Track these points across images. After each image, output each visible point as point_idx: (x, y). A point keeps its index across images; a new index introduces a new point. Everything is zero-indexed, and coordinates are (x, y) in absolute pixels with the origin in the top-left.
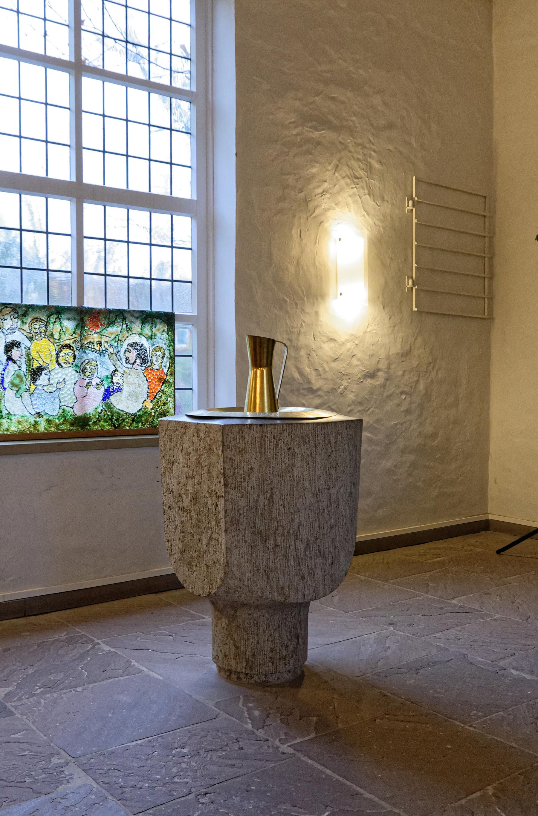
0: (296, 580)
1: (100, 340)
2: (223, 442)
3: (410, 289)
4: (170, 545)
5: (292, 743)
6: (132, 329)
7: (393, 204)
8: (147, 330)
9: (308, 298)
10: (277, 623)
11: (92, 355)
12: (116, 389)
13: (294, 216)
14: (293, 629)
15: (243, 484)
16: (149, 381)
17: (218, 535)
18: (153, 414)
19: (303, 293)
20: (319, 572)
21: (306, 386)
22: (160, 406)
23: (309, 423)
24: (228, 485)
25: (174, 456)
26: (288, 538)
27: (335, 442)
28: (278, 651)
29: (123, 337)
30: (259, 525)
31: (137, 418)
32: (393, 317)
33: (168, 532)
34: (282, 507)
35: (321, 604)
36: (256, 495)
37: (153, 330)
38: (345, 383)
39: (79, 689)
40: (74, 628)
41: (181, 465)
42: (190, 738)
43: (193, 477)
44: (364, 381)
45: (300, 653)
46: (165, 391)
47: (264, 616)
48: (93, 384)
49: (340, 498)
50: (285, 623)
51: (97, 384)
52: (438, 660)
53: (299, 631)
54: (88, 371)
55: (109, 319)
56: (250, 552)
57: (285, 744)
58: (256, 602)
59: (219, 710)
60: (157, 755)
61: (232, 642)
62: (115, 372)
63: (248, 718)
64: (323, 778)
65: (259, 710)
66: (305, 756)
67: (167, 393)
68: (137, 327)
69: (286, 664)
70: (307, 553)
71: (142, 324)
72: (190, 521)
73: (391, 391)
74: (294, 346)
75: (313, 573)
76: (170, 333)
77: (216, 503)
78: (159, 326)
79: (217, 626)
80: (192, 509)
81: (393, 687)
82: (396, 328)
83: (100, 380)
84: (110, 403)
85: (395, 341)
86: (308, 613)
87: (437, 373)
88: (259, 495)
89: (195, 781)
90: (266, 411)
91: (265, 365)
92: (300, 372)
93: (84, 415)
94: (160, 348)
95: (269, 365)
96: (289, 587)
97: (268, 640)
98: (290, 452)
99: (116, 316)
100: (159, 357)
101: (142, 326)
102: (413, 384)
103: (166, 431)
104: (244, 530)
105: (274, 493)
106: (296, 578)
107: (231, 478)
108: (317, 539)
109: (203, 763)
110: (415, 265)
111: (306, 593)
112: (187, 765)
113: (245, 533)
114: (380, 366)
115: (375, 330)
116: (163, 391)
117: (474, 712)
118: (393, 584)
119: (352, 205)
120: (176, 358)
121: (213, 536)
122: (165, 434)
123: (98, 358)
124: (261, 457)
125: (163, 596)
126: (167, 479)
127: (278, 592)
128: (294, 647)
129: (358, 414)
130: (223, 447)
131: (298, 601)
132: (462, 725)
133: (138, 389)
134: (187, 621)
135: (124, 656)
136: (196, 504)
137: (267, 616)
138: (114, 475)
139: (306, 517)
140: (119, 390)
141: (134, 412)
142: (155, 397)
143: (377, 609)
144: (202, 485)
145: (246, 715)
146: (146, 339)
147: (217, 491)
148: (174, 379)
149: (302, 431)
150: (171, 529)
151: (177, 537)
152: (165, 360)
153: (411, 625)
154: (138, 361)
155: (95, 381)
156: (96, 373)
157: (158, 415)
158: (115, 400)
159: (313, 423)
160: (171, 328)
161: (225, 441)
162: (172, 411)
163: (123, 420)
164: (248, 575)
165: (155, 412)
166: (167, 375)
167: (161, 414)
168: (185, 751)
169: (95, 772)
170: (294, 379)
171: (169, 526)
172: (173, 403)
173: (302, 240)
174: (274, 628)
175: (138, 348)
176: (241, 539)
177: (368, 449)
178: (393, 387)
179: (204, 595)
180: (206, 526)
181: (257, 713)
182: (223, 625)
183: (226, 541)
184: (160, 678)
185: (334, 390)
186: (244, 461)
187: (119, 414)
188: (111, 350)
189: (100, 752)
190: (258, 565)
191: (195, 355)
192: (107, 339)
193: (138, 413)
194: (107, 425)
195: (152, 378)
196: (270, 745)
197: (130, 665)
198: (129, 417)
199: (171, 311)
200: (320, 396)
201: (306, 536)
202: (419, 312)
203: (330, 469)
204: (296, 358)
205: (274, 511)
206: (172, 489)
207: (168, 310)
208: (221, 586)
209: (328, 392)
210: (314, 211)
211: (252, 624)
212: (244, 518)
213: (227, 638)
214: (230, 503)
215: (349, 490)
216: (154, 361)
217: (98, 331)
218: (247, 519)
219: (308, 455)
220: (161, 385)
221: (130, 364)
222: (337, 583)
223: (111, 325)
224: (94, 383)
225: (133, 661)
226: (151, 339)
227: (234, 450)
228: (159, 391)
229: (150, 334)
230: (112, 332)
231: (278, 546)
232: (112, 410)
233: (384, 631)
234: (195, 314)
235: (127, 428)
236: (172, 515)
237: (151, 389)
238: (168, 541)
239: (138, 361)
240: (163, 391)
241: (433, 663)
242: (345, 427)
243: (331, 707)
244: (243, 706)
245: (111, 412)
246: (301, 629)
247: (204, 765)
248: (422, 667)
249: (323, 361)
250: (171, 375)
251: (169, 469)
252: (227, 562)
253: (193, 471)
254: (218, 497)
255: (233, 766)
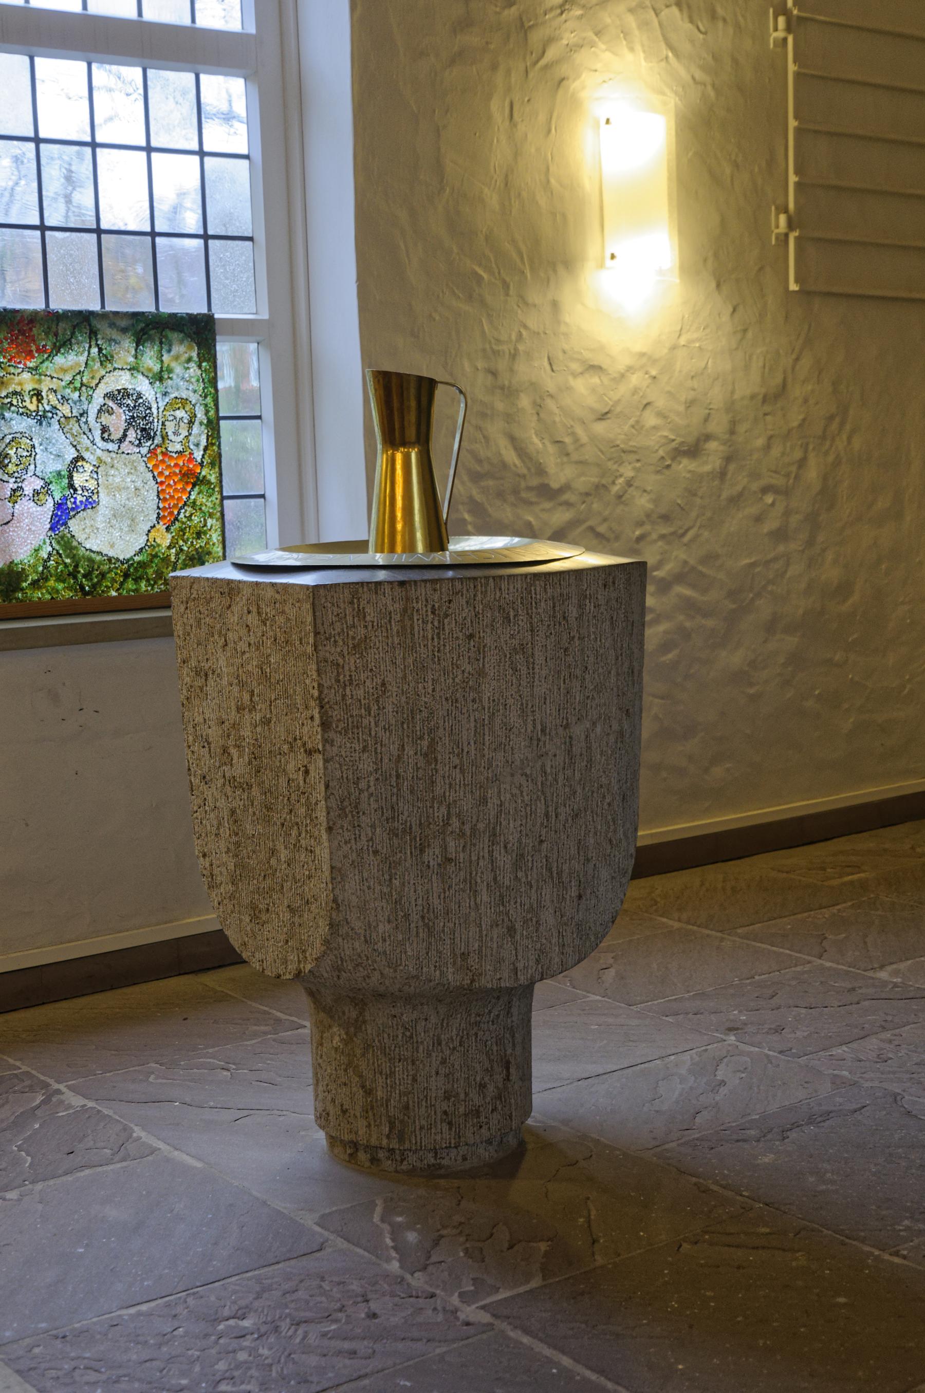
0: (495, 936)
1: (36, 386)
3: (782, 238)
4: (207, 865)
6: (112, 357)
8: (150, 360)
10: (457, 1035)
11: (20, 424)
12: (81, 502)
13: (494, 67)
14: (495, 1048)
16: (159, 480)
18: (173, 558)
20: (548, 918)
21: (535, 482)
22: (188, 539)
24: (331, 723)
25: (207, 660)
26: (474, 841)
27: (579, 618)
28: (462, 1096)
29: (93, 378)
30: (406, 813)
31: (136, 569)
33: (203, 835)
34: (458, 770)
35: (574, 988)
36: (396, 746)
37: (164, 358)
38: (628, 472)
39: (12, 1195)
40: (5, 1057)
41: (225, 682)
42: (258, 1296)
43: (253, 709)
44: (674, 466)
45: (513, 1101)
46: (198, 503)
47: (426, 1020)
48: (26, 493)
49: (594, 746)
50: (476, 1034)
51: (36, 493)
53: (509, 1051)
54: (13, 461)
55: (56, 335)
56: (387, 877)
57: (474, 1303)
59: (326, 1233)
60: (182, 1333)
62: (77, 462)
63: (392, 1247)
64: (553, 1374)
65: (415, 1230)
66: (516, 1327)
67: (203, 508)
68: (125, 351)
69: (481, 1127)
70: (520, 874)
71: (137, 346)
73: (739, 488)
74: (502, 388)
75: (534, 919)
76: (204, 364)
77: (306, 766)
78: (178, 349)
79: (322, 1045)
80: (253, 780)
82: (750, 335)
83: (42, 483)
84: (69, 535)
85: (747, 368)
88: (403, 745)
90: (420, 547)
93: (9, 566)
95: (423, 440)
96: (480, 951)
97: (437, 1073)
98: (472, 643)
99: (74, 327)
100: (182, 424)
101: (136, 350)
102: (794, 469)
104: (371, 826)
106: (495, 932)
108: (541, 841)
109: (285, 1349)
111: (520, 965)
112: (250, 1356)
113: (373, 834)
114: (712, 427)
115: (698, 340)
116: (194, 502)
117: (906, 1222)
119: (636, 32)
120: (222, 423)
121: (303, 842)
122: (187, 608)
124: (404, 658)
127: (454, 963)
128: (497, 1087)
129: (660, 543)
132: (877, 1253)
133: (134, 503)
134: (265, 1033)
135: (117, 1118)
137: (433, 1019)
138: (84, 707)
139: (515, 791)
140: (90, 504)
141: (128, 556)
142: (176, 519)
143: (703, 995)
145: (389, 1242)
146: (147, 382)
147: (305, 738)
148: (221, 474)
149: (498, 594)
150: (209, 828)
151: (223, 845)
152: (196, 429)
153: (779, 1030)
154: (132, 435)
155: (31, 485)
156: (32, 467)
157: (184, 560)
158: (81, 528)
159: (526, 575)
160: (208, 354)
161: (319, 621)
162: (218, 549)
163: (103, 575)
165: (177, 554)
166: (201, 464)
167: (192, 559)
168: (246, 1323)
169: (44, 1375)
170: (504, 465)
171: (204, 822)
173: (515, 126)
174: (451, 1046)
175: (129, 402)
177: (688, 624)
179: (288, 977)
180: (285, 820)
181: (412, 1237)
182: (334, 1042)
183: (331, 853)
184: (199, 1165)
185: (600, 489)
186: (365, 667)
187: (91, 560)
188: (65, 410)
189: (54, 1332)
190: (407, 905)
191: (268, 414)
192: (54, 384)
193: (137, 558)
194: (64, 588)
195: (167, 473)
197: (131, 1136)
198: (116, 568)
199: (204, 310)
200: (568, 504)
201: (517, 835)
205: (439, 780)
206: (207, 735)
207: (199, 308)
208: (324, 954)
209: (588, 494)
210: (544, 53)
211: (400, 1037)
213: (345, 1070)
214: (338, 766)
216: (170, 433)
217: (31, 364)
218: (377, 801)
219: (515, 649)
220: (189, 489)
221: (112, 441)
222: (593, 939)
223: (62, 351)
224: (28, 490)
225: (136, 1128)
226: (161, 379)
227: (341, 643)
228: (185, 504)
229: (157, 368)
230: (65, 367)
231: (450, 860)
234: (265, 315)
235: (114, 594)
236: (210, 797)
237: (165, 500)
238: (204, 856)
239: (132, 435)
240: (194, 502)
242: (600, 583)
243: (582, 1220)
244: (383, 1220)
245: (73, 557)
246: (514, 1045)
248: (795, 1125)
249: (573, 420)
250: (212, 464)
251: (198, 690)
252: (335, 900)
253: (252, 694)
254: (309, 753)
255: (353, 1353)
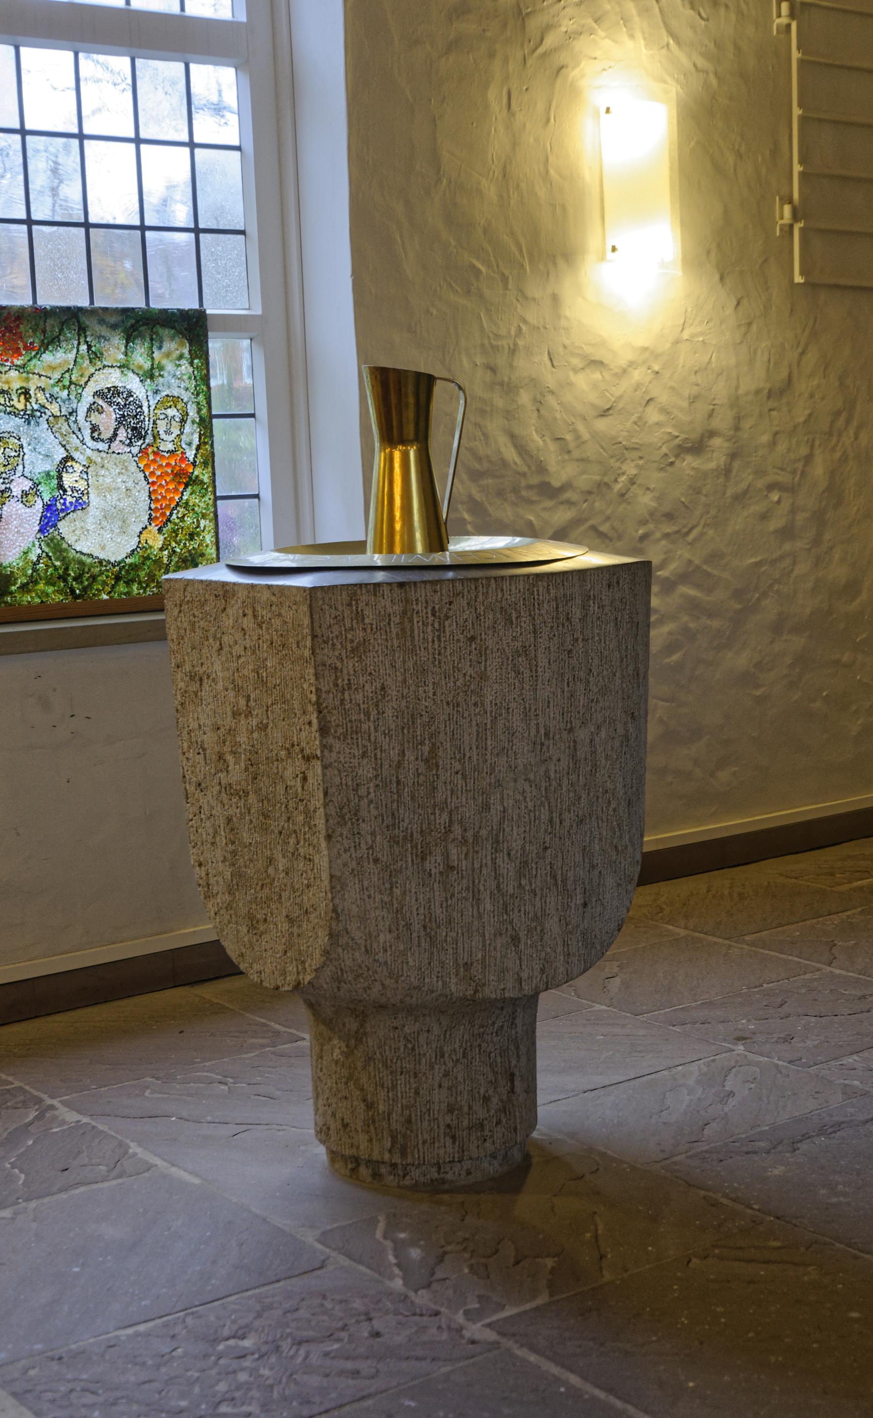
0: (499, 946)
1: (24, 385)
2: (313, 630)
3: (787, 229)
4: (203, 874)
5: (494, 1318)
6: (102, 354)
7: (740, 12)
8: (140, 357)
9: (531, 262)
10: (460, 1047)
12: (71, 503)
13: (492, 55)
15: (365, 727)
16: (150, 480)
17: (311, 849)
18: (165, 560)
19: (521, 251)
20: (553, 925)
21: (535, 480)
22: (180, 541)
23: (516, 576)
25: (202, 664)
27: (583, 619)
28: (466, 1109)
29: (82, 376)
30: (407, 821)
31: (127, 572)
32: (745, 301)
33: (199, 844)
34: (460, 776)
35: (579, 997)
36: (397, 751)
38: (630, 469)
41: (220, 686)
42: (259, 1315)
43: (249, 714)
44: (677, 463)
45: (518, 1114)
46: (191, 504)
48: (15, 494)
49: (599, 750)
50: (480, 1046)
51: (25, 494)
52: (844, 1119)
53: (514, 1062)
55: (44, 332)
56: (387, 886)
58: (408, 999)
59: (327, 1250)
61: (358, 1093)
62: (66, 462)
64: (562, 1394)
67: (196, 509)
69: (485, 1140)
70: (523, 882)
71: (127, 343)
72: (247, 818)
73: (743, 486)
74: (502, 384)
75: (539, 928)
76: (196, 361)
77: (304, 773)
78: (170, 345)
79: (321, 1057)
80: (250, 787)
81: (736, 1185)
82: (754, 327)
83: (30, 484)
85: (751, 362)
86: (535, 1021)
87: (856, 436)
89: (267, 1411)
90: (419, 548)
91: (411, 436)
92: (521, 449)
94: (175, 400)
97: (440, 1086)
98: (474, 646)
99: (63, 324)
100: (173, 423)
101: (126, 347)
102: (800, 465)
103: (181, 606)
105: (438, 744)
107: (335, 712)
110: (797, 168)
111: (524, 975)
112: (251, 1376)
113: (373, 841)
114: (716, 423)
115: (701, 334)
116: (187, 503)
118: (752, 944)
119: (637, 19)
120: (214, 421)
121: (301, 851)
122: (180, 612)
123: (24, 428)
124: (404, 661)
125: (207, 992)
126: (191, 720)
128: (501, 1100)
129: (664, 542)
130: (313, 639)
131: (507, 995)
133: (125, 503)
136: (259, 777)
139: (519, 797)
140: (81, 505)
141: (119, 558)
142: (169, 520)
143: (710, 1004)
144: (269, 730)
145: (392, 1259)
146: (138, 379)
148: (214, 474)
149: (500, 595)
150: (204, 836)
151: (219, 854)
152: (188, 428)
154: (122, 434)
156: (20, 468)
157: (177, 562)
159: (528, 576)
161: (316, 625)
162: (211, 551)
163: (94, 578)
164: (385, 938)
165: (170, 556)
166: (194, 464)
167: (184, 561)
168: (247, 1343)
170: (504, 463)
171: (200, 831)
172: (212, 533)
173: (513, 115)
175: (120, 400)
176: (366, 856)
177: (692, 625)
178: (749, 474)
179: (287, 988)
180: (283, 827)
182: (335, 1054)
183: (330, 861)
184: (197, 1181)
185: (602, 487)
187: (81, 563)
188: (54, 408)
189: (50, 1354)
191: (262, 411)
192: (43, 382)
193: (128, 561)
194: (54, 592)
195: (158, 473)
196: (444, 1322)
197: (126, 1153)
198: (107, 571)
199: (196, 306)
200: (569, 503)
201: (520, 842)
202: (811, 286)
203: (571, 685)
204: (508, 412)
205: (440, 785)
206: (202, 742)
208: (324, 965)
209: (590, 493)
210: (542, 40)
211: (402, 1049)
212: (369, 806)
213: (346, 1083)
214: (336, 772)
215: (621, 730)
217: (18, 362)
218: (377, 808)
219: (517, 651)
220: (181, 490)
221: (102, 441)
222: (598, 948)
223: (50, 348)
224: (16, 491)
225: (132, 1144)
226: (152, 377)
227: (340, 647)
228: (178, 505)
229: (147, 365)
230: (53, 365)
231: (452, 868)
232: (65, 554)
233: (724, 1055)
234: (258, 311)
235: (105, 597)
237: (157, 500)
238: (200, 865)
239: (122, 434)
240: (187, 503)
241: (832, 1127)
242: (605, 582)
243: (588, 1235)
244: (385, 1237)
245: (63, 560)
246: (518, 1057)
247: (288, 1373)
248: (805, 1137)
250: (205, 464)
251: (193, 696)
252: (335, 910)
253: (248, 700)
254: (307, 759)
